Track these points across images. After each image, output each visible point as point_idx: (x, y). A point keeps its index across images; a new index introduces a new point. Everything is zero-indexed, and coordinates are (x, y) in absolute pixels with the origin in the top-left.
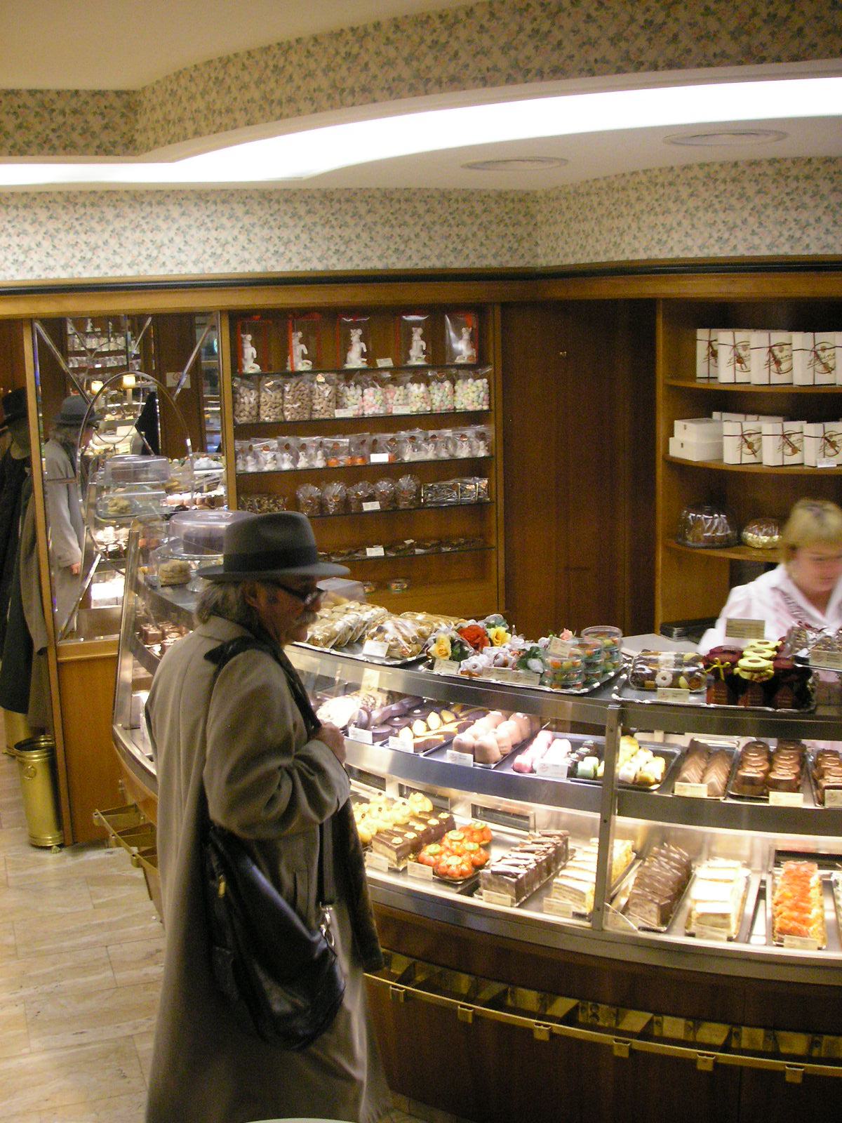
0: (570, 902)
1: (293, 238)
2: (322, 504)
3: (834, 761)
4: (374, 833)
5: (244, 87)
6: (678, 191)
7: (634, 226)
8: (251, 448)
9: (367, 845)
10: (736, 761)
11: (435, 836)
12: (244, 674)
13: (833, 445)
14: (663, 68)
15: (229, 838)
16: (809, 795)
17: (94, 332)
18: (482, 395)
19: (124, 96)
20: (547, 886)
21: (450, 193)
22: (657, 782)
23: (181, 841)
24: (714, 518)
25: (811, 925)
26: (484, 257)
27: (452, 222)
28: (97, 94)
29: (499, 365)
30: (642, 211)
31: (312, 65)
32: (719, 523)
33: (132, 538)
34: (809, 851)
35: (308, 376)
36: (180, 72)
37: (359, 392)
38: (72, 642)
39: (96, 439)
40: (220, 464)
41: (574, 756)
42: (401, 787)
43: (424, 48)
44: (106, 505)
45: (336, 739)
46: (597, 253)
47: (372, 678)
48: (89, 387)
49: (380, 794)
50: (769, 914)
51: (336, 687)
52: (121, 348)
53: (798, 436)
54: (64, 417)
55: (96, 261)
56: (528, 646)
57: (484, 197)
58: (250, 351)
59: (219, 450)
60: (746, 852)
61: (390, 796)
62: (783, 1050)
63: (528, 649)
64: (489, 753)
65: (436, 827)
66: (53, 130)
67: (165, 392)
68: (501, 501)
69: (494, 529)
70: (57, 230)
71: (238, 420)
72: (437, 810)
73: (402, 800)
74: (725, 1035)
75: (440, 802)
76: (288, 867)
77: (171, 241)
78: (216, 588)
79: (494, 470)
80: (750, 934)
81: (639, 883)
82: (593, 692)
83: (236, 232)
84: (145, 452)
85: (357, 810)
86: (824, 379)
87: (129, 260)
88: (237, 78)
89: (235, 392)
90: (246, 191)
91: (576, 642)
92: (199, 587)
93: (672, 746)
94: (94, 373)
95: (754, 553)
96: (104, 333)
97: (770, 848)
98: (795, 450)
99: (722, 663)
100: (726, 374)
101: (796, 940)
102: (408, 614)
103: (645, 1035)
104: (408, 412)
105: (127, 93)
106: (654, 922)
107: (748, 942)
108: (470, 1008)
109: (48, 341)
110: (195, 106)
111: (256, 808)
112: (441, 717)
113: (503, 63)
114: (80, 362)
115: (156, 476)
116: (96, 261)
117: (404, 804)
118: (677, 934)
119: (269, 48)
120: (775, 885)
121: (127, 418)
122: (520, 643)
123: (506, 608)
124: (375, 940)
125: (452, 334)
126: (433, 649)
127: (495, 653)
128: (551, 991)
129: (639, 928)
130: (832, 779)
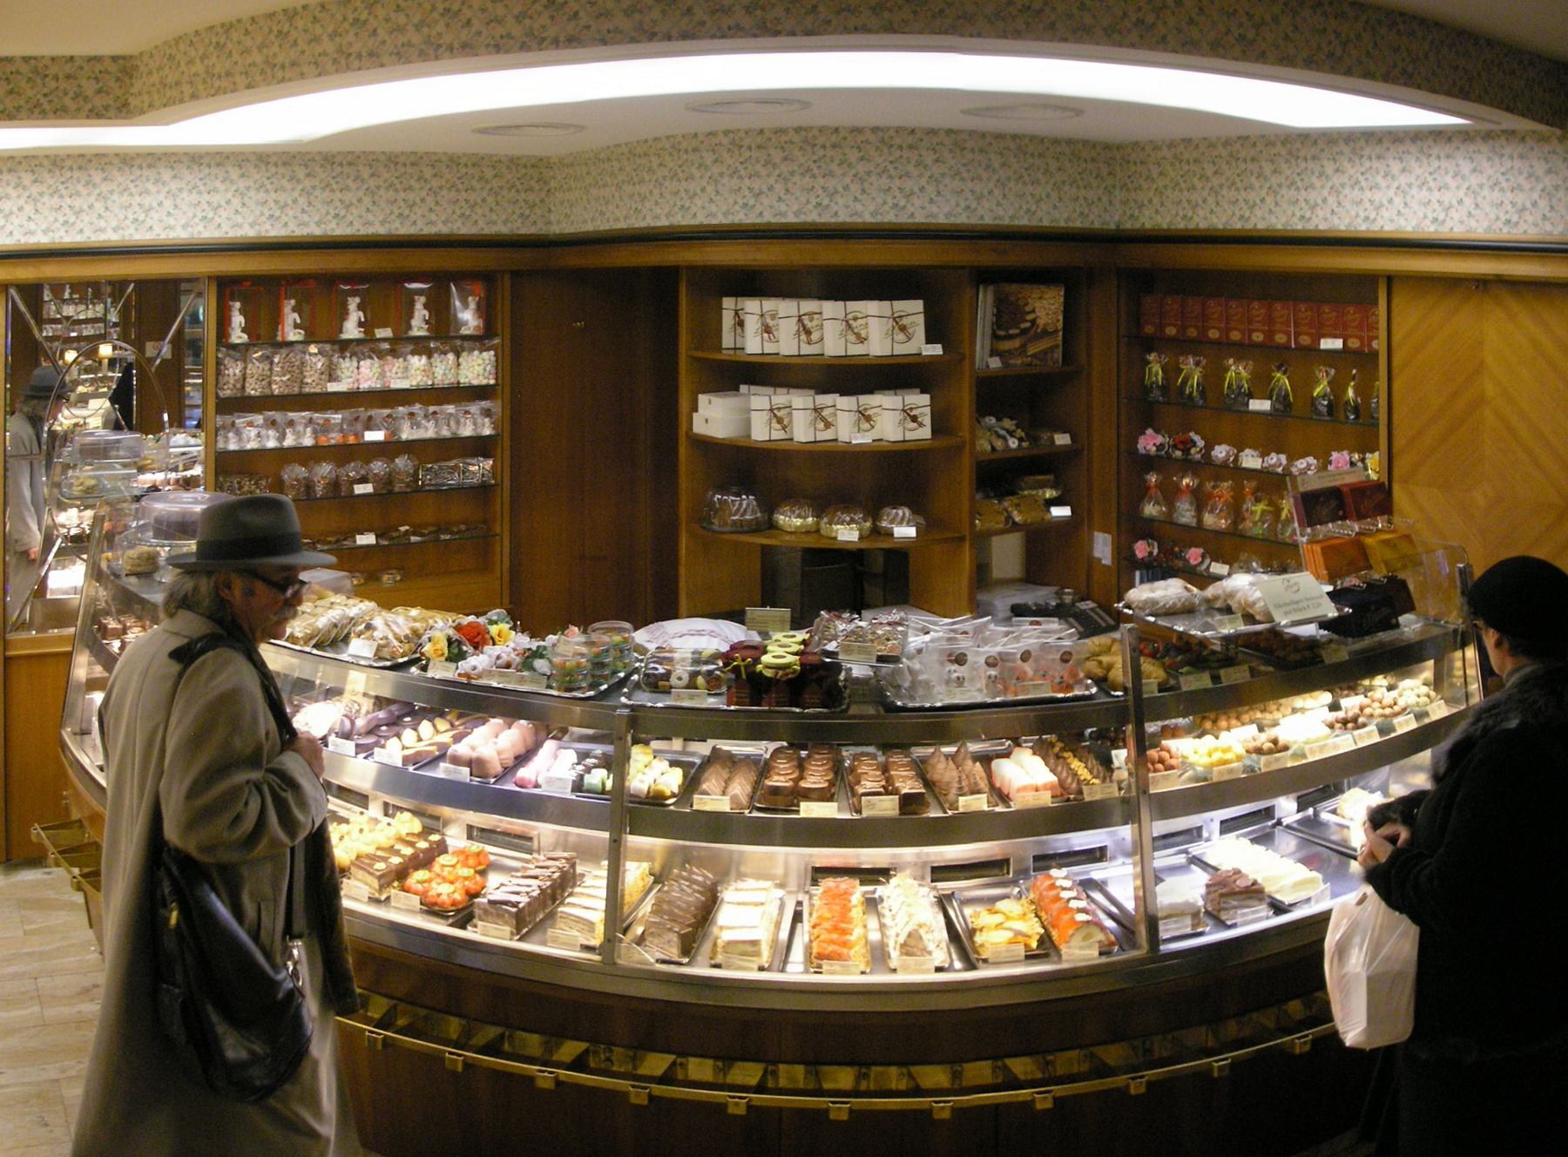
0: (577, 934)
1: (290, 202)
2: (309, 486)
3: (871, 765)
4: (353, 858)
5: (246, 51)
6: (702, 157)
7: (656, 192)
8: (233, 424)
9: (344, 871)
10: (763, 768)
11: (424, 860)
12: (213, 675)
13: (868, 419)
14: (677, 39)
15: (185, 861)
16: (845, 804)
17: (71, 299)
18: (488, 368)
19: (121, 61)
20: (551, 916)
21: (459, 157)
22: (673, 795)
23: (129, 862)
24: (742, 500)
25: (851, 948)
26: (494, 223)
27: (460, 186)
28: (92, 59)
29: (508, 336)
30: (664, 177)
31: (318, 30)
32: (748, 505)
33: (97, 521)
34: (851, 865)
35: (300, 347)
36: (180, 38)
37: (355, 364)
38: (23, 635)
39: (66, 412)
40: (199, 441)
41: (581, 767)
42: (386, 805)
43: (435, 15)
44: (71, 485)
45: (313, 751)
46: (617, 220)
47: (357, 681)
48: (62, 356)
49: (362, 813)
50: (806, 938)
51: (316, 692)
52: (99, 315)
53: (831, 410)
54: (33, 388)
55: (79, 225)
56: (534, 645)
57: (495, 162)
58: (238, 320)
59: (198, 426)
60: (780, 871)
61: (374, 816)
62: (827, 1086)
63: (534, 648)
64: (488, 766)
65: (425, 851)
66: (45, 95)
67: (143, 364)
68: (507, 483)
69: (499, 515)
70: (41, 194)
71: (221, 394)
72: (426, 832)
73: (387, 820)
74: (760, 1074)
75: (429, 822)
76: (252, 894)
77: (160, 204)
78: (187, 578)
79: (499, 450)
80: (785, 962)
81: (657, 910)
82: (602, 696)
83: (229, 195)
84: (117, 427)
85: (334, 831)
86: (856, 350)
87: (114, 224)
88: (239, 42)
89: (219, 363)
90: (242, 153)
91: (582, 639)
92: (167, 577)
93: (693, 754)
94: (68, 342)
95: (787, 538)
96: (83, 300)
97: (806, 865)
98: (828, 425)
99: (743, 660)
100: (753, 344)
101: (836, 966)
102: (400, 609)
103: (666, 1079)
104: (408, 387)
105: (124, 58)
106: (674, 952)
107: (783, 970)
108: (460, 1055)
109: (22, 308)
110: (193, 70)
111: (218, 828)
112: (434, 726)
113: (517, 31)
114: (54, 330)
115: (128, 454)
116: (79, 225)
117: (389, 824)
118: (700, 966)
119: (274, 14)
120: (812, 905)
121: (101, 390)
122: (524, 641)
123: (511, 603)
124: (350, 979)
125: (458, 303)
126: (427, 648)
127: (497, 653)
128: (557, 1033)
129: (657, 961)
130: (869, 784)
